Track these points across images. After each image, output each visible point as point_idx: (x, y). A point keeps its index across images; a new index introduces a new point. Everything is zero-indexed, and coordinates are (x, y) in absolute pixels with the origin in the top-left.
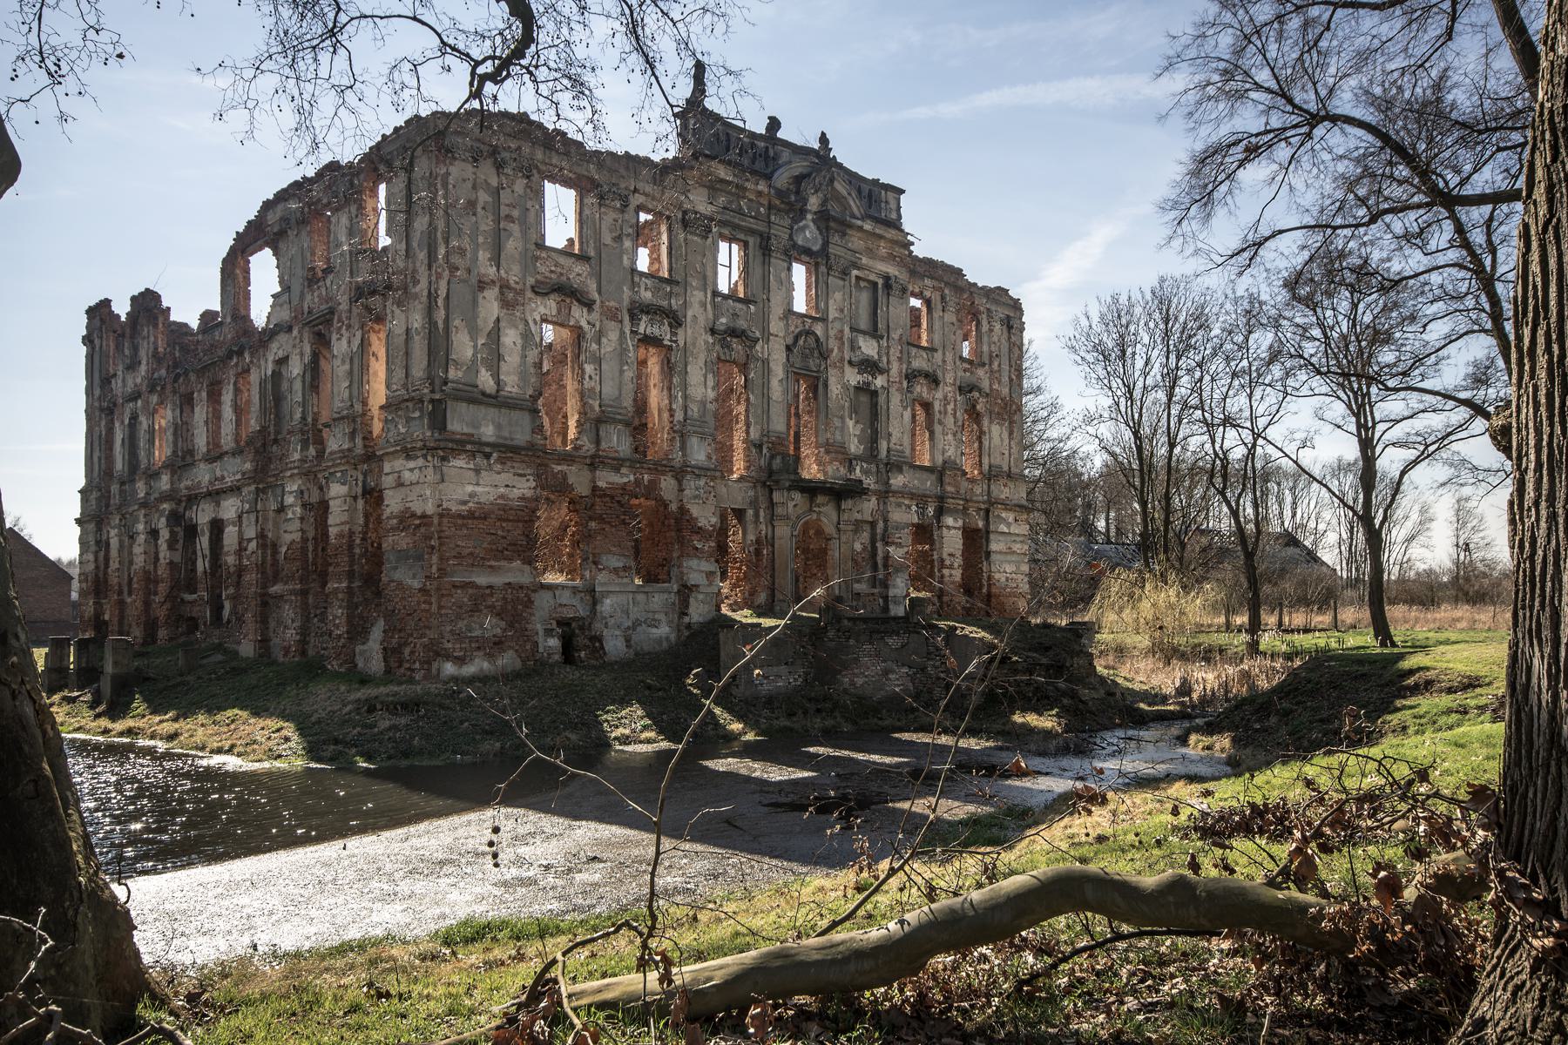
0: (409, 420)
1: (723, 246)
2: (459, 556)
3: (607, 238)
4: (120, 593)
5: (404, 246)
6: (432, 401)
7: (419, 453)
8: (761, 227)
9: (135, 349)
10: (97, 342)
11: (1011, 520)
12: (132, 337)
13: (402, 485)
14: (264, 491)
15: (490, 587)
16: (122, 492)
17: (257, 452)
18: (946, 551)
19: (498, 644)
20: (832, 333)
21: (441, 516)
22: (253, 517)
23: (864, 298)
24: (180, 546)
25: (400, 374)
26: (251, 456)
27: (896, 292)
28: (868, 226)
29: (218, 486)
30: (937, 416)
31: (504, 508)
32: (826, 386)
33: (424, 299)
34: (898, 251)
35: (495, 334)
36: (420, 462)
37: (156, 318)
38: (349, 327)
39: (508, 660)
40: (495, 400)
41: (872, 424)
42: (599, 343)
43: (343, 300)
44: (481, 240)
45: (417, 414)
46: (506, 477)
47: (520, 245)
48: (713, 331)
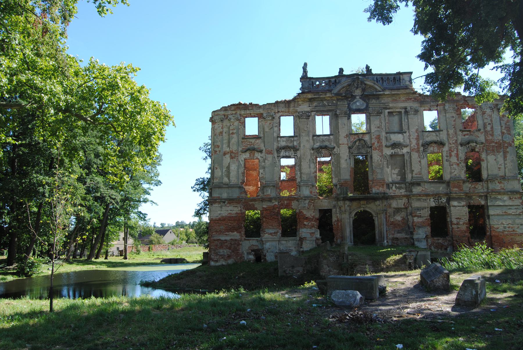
2: (216, 232)
3: (267, 130)
19: (229, 257)
23: (396, 119)
28: (387, 92)
32: (371, 157)
34: (411, 96)
35: (228, 167)
40: (229, 186)
42: (264, 162)
44: (224, 142)
47: (236, 140)
48: (313, 149)
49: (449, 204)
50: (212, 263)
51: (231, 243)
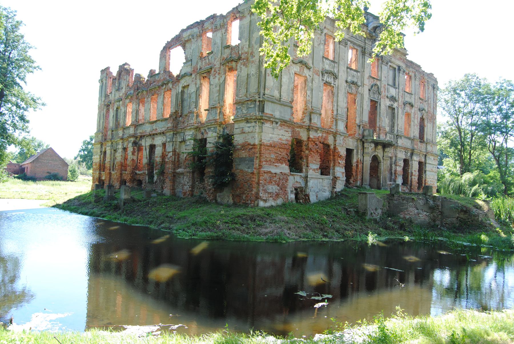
0: (248, 108)
1: (350, 51)
2: (266, 161)
4: (110, 170)
5: (248, 43)
6: (259, 101)
7: (253, 121)
8: (362, 44)
9: (120, 84)
10: (104, 82)
11: (433, 159)
12: (119, 79)
13: (244, 133)
14: (176, 134)
15: (276, 173)
16: (112, 134)
17: (174, 120)
18: (413, 169)
20: (382, 85)
21: (261, 145)
22: (171, 144)
23: (391, 73)
24: (136, 154)
25: (243, 91)
26: (171, 121)
27: (401, 72)
29: (154, 132)
30: (412, 119)
31: (281, 144)
32: (380, 105)
33: (257, 63)
34: (403, 57)
36: (253, 124)
37: (129, 73)
38: (219, 74)
39: (280, 201)
41: (392, 120)
43: (217, 65)
45: (253, 106)
46: (282, 132)
49: (411, 158)
50: (262, 204)
51: (280, 178)
